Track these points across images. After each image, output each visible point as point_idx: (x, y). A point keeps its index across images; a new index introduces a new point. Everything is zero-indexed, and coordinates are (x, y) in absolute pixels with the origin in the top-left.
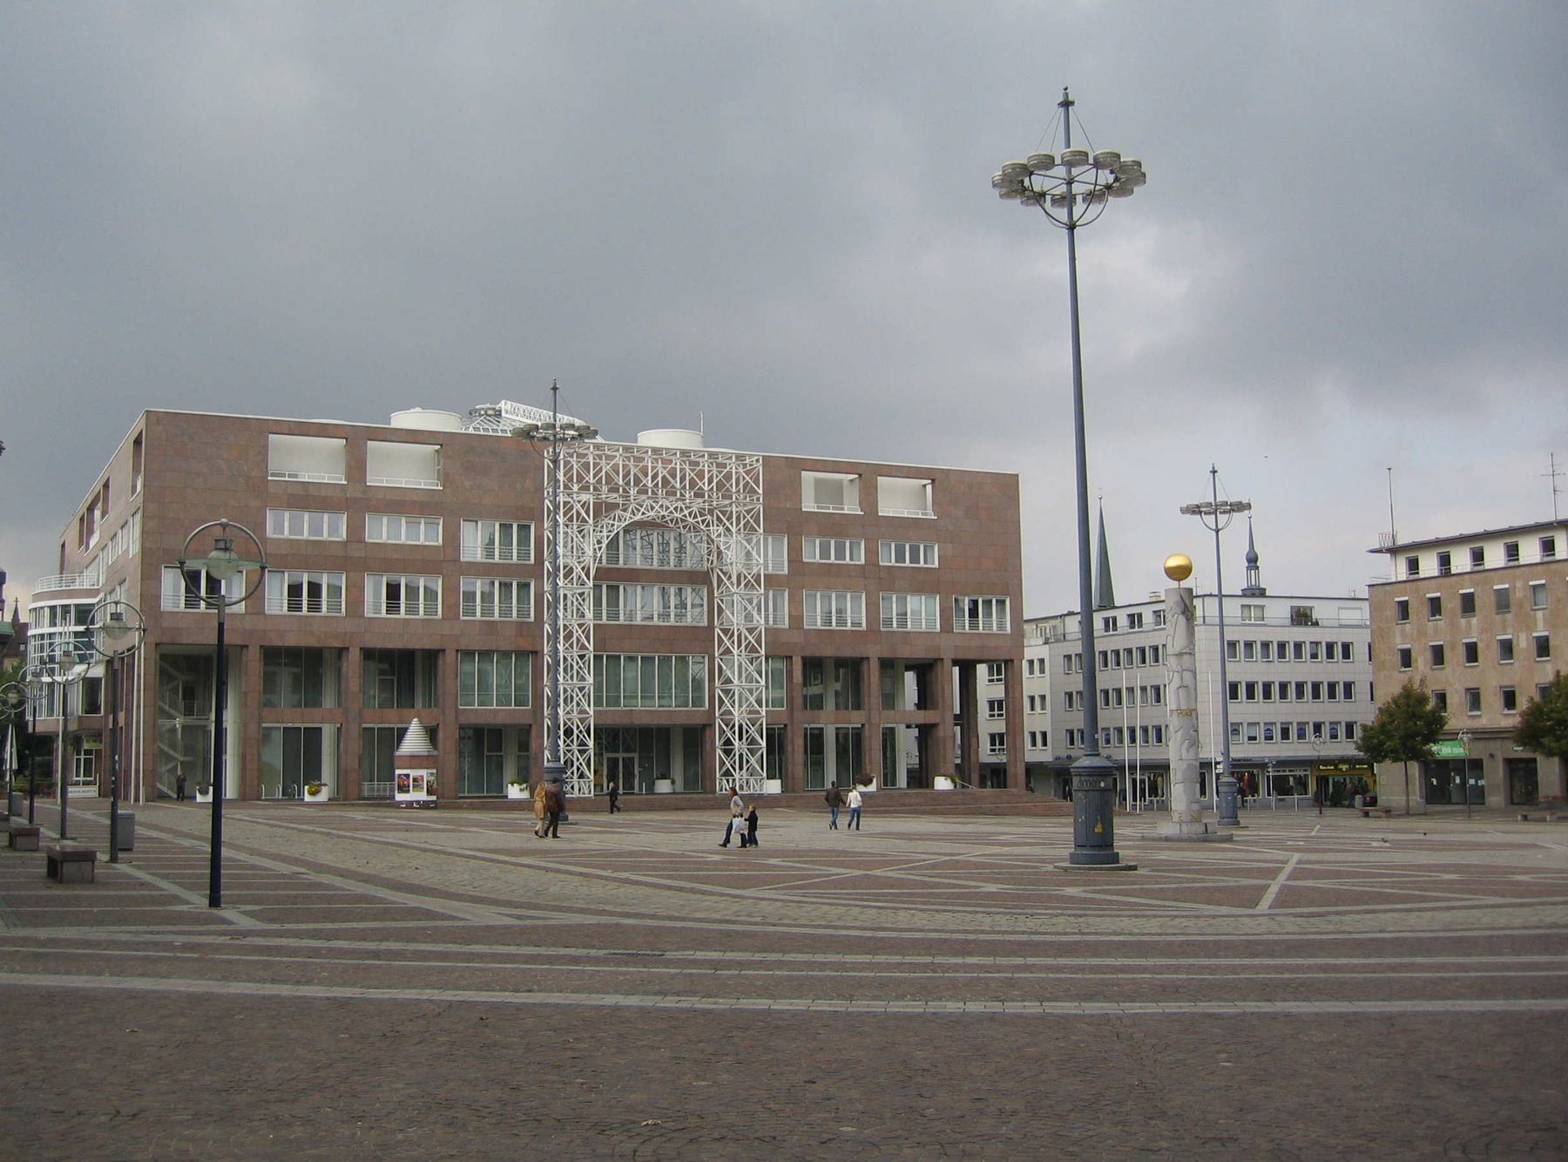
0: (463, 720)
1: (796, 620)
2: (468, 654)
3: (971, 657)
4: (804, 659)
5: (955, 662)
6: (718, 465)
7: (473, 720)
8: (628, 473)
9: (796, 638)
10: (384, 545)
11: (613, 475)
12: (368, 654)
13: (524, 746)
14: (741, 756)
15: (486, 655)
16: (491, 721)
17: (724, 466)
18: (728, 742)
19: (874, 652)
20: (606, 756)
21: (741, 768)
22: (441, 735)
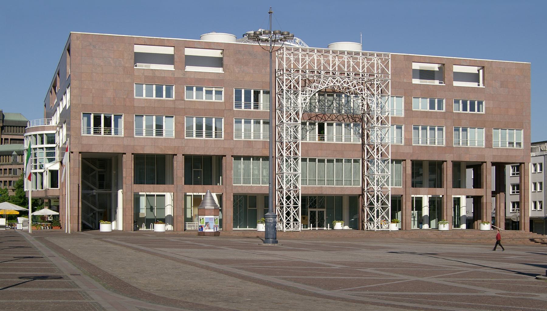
0: (235, 191)
1: (408, 141)
2: (237, 158)
3: (502, 161)
4: (188, 158)
5: (493, 164)
6: (368, 59)
7: (241, 191)
8: (335, 64)
9: (408, 150)
10: (395, 117)
11: (326, 65)
12: (188, 158)
13: (266, 205)
14: (378, 211)
15: (247, 158)
16: (250, 192)
17: (371, 60)
18: (371, 204)
19: (449, 158)
20: (309, 210)
21: (378, 217)
22: (224, 199)
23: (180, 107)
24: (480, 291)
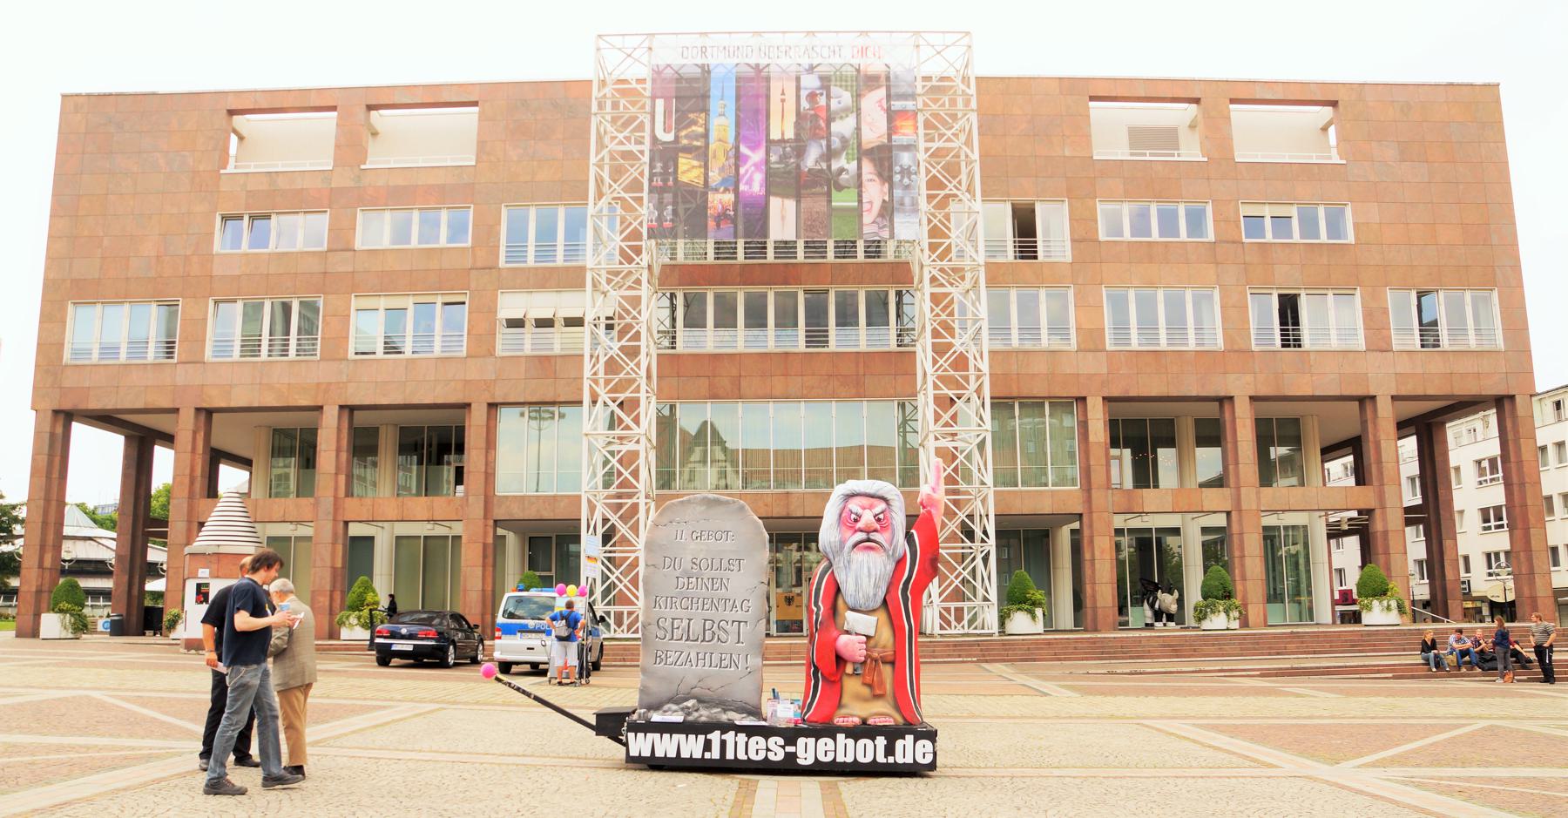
9: (1093, 365)
23: (341, 269)
24: (1439, 790)
